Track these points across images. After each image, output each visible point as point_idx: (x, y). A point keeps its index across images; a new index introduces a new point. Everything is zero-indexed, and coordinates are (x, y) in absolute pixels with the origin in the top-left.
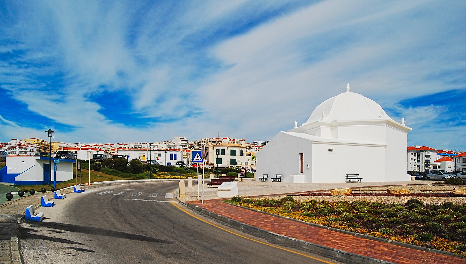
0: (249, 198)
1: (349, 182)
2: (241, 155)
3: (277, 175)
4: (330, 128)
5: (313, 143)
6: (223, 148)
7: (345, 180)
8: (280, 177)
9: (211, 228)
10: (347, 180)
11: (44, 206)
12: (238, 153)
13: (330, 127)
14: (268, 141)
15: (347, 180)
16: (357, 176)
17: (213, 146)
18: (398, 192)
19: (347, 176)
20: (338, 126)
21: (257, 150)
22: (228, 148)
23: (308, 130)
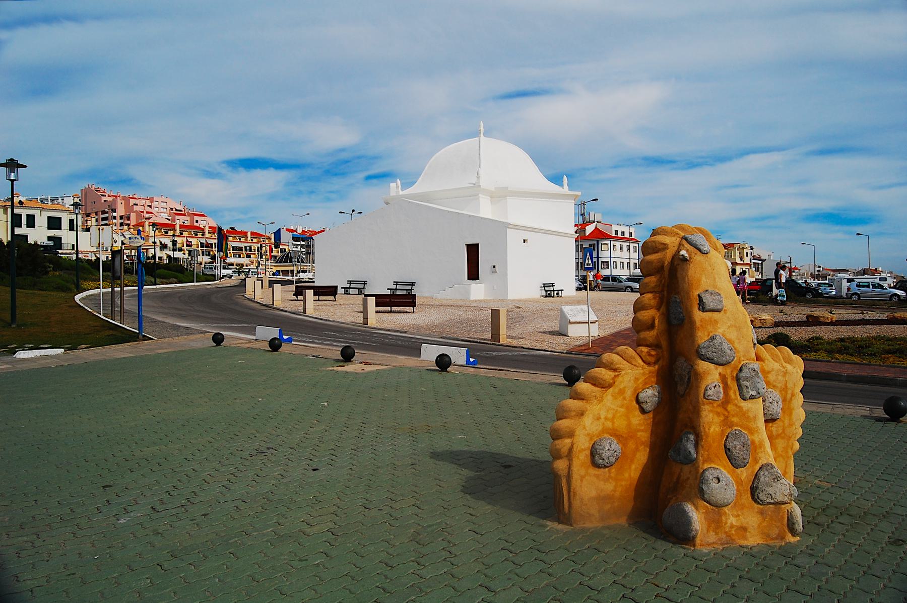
0: (878, 363)
1: (549, 296)
2: (72, 228)
3: (350, 281)
4: (491, 200)
5: (508, 228)
6: (31, 212)
7: (537, 293)
8: (410, 287)
9: (582, 474)
10: (543, 293)
11: (804, 517)
12: (65, 224)
13: (491, 198)
14: (43, 197)
15: (543, 293)
16: (553, 286)
17: (5, 206)
18: (829, 319)
19: (544, 286)
20: (508, 197)
21: (725, 246)
22: (42, 212)
23: (441, 199)
